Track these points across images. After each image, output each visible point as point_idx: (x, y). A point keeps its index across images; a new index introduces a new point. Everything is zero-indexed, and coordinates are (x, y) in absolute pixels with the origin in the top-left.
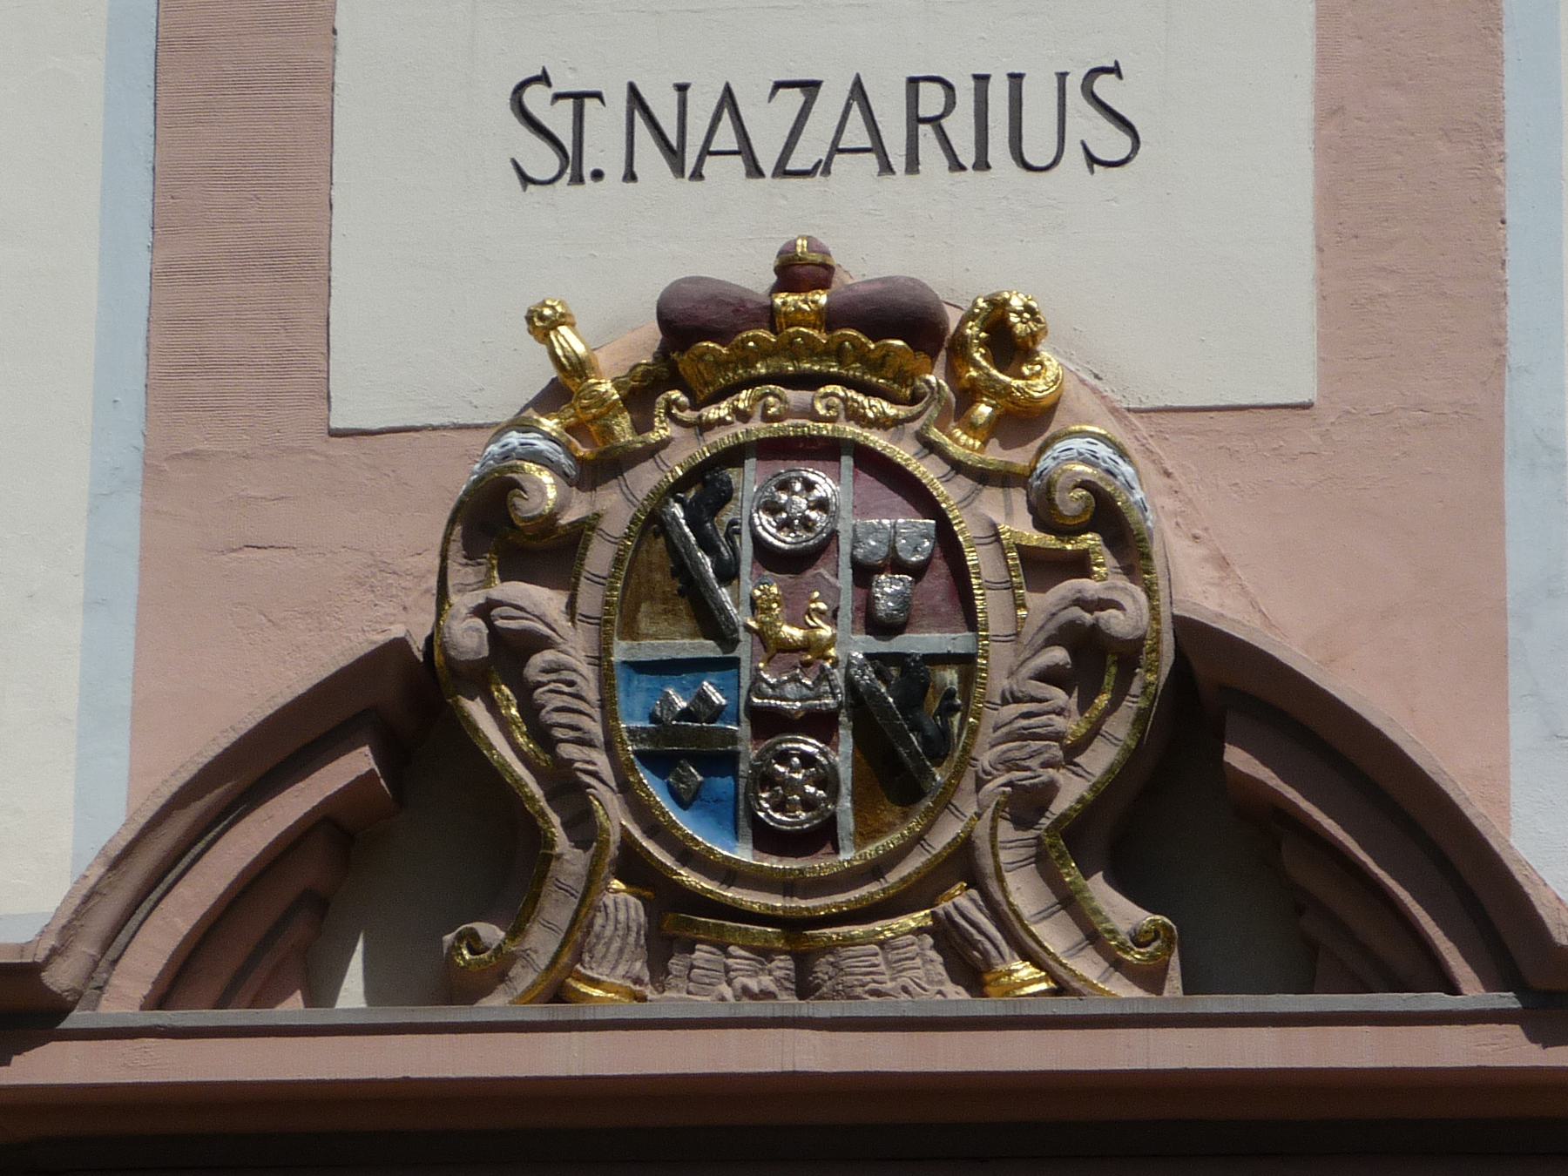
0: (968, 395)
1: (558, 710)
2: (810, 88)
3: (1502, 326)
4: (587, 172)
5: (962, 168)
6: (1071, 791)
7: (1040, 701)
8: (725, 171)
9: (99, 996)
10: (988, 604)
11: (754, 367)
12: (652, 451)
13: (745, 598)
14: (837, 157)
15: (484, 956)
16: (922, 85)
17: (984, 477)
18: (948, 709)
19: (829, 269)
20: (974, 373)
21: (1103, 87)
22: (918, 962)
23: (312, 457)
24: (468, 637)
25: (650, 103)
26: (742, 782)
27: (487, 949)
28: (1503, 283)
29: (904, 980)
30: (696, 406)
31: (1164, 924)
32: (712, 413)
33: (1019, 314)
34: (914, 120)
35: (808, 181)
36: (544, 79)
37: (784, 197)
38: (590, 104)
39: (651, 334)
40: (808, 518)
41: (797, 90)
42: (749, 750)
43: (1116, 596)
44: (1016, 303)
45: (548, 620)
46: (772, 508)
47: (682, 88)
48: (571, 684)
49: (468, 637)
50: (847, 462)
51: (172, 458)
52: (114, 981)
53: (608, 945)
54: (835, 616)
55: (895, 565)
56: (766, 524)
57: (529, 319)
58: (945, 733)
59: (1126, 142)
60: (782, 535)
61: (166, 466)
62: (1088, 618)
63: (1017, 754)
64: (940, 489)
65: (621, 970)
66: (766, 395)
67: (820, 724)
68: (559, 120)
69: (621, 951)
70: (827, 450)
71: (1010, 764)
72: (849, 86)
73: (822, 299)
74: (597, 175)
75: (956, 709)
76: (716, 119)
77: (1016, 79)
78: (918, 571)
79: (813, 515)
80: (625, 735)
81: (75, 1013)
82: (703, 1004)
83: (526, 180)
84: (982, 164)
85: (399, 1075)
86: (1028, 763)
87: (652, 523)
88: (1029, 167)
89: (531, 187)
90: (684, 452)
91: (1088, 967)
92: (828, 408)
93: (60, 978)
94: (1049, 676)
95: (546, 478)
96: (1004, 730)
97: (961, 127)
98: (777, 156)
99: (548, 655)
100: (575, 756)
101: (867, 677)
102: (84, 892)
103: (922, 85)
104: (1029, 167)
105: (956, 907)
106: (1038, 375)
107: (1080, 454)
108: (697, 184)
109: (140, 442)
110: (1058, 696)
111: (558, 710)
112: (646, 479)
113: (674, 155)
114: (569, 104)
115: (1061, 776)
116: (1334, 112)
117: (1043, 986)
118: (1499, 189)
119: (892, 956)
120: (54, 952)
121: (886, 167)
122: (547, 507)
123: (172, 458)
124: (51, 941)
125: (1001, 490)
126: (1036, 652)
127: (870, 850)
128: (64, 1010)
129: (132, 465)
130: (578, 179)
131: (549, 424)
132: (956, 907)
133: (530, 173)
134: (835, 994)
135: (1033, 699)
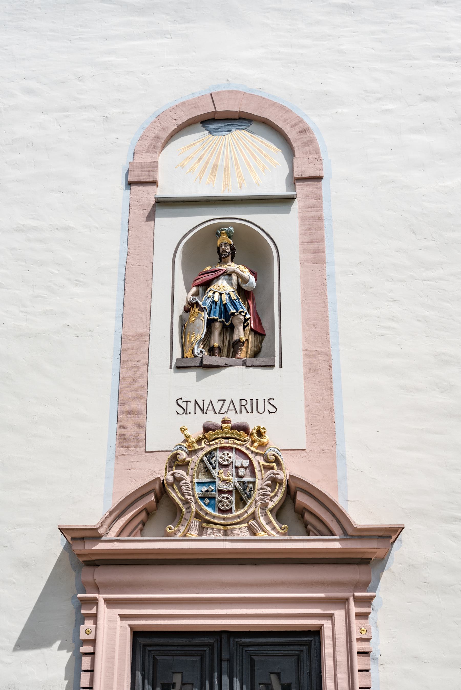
0: (253, 442)
1: (185, 490)
4: (188, 413)
5: (249, 413)
6: (271, 505)
8: (211, 413)
9: (107, 535)
10: (258, 474)
11: (219, 435)
12: (202, 449)
13: (217, 472)
14: (228, 411)
15: (172, 530)
16: (242, 400)
17: (257, 454)
18: (251, 490)
19: (231, 421)
20: (255, 438)
21: (271, 401)
22: (245, 532)
23: (143, 455)
24: (170, 479)
25: (198, 402)
26: (216, 502)
27: (172, 529)
30: (209, 442)
31: (286, 526)
32: (211, 443)
33: (262, 429)
35: (224, 414)
36: (181, 399)
37: (220, 417)
39: (202, 431)
40: (228, 459)
41: (222, 401)
42: (218, 498)
43: (279, 473)
44: (262, 427)
45: (184, 475)
46: (222, 458)
47: (203, 400)
48: (188, 486)
49: (170, 479)
50: (234, 450)
52: (110, 532)
53: (193, 528)
54: (232, 475)
55: (242, 467)
56: (221, 460)
57: (181, 429)
58: (250, 495)
59: (275, 410)
60: (223, 462)
61: (119, 456)
62: (274, 476)
63: (262, 498)
66: (220, 440)
67: (229, 492)
68: (184, 405)
69: (195, 529)
70: (231, 449)
71: (261, 499)
73: (230, 425)
74: (190, 413)
75: (252, 490)
76: (209, 405)
78: (246, 468)
79: (229, 459)
80: (197, 494)
81: (103, 537)
83: (178, 414)
85: (158, 548)
86: (264, 499)
87: (202, 461)
89: (179, 415)
90: (207, 449)
91: (273, 533)
92: (231, 442)
93: (101, 531)
94: (267, 485)
95: (184, 453)
96: (261, 494)
97: (248, 407)
98: (219, 410)
99: (184, 481)
100: (188, 497)
102: (105, 517)
103: (242, 400)
105: (252, 523)
106: (265, 439)
107: (273, 450)
108: (206, 415)
110: (269, 489)
111: (185, 490)
112: (201, 454)
113: (202, 410)
115: (270, 502)
116: (307, 406)
118: (334, 418)
119: (241, 530)
120: (100, 527)
122: (184, 458)
124: (100, 525)
125: (259, 457)
128: (101, 537)
129: (113, 456)
131: (185, 445)
132: (252, 523)
133: (179, 413)
135: (265, 489)
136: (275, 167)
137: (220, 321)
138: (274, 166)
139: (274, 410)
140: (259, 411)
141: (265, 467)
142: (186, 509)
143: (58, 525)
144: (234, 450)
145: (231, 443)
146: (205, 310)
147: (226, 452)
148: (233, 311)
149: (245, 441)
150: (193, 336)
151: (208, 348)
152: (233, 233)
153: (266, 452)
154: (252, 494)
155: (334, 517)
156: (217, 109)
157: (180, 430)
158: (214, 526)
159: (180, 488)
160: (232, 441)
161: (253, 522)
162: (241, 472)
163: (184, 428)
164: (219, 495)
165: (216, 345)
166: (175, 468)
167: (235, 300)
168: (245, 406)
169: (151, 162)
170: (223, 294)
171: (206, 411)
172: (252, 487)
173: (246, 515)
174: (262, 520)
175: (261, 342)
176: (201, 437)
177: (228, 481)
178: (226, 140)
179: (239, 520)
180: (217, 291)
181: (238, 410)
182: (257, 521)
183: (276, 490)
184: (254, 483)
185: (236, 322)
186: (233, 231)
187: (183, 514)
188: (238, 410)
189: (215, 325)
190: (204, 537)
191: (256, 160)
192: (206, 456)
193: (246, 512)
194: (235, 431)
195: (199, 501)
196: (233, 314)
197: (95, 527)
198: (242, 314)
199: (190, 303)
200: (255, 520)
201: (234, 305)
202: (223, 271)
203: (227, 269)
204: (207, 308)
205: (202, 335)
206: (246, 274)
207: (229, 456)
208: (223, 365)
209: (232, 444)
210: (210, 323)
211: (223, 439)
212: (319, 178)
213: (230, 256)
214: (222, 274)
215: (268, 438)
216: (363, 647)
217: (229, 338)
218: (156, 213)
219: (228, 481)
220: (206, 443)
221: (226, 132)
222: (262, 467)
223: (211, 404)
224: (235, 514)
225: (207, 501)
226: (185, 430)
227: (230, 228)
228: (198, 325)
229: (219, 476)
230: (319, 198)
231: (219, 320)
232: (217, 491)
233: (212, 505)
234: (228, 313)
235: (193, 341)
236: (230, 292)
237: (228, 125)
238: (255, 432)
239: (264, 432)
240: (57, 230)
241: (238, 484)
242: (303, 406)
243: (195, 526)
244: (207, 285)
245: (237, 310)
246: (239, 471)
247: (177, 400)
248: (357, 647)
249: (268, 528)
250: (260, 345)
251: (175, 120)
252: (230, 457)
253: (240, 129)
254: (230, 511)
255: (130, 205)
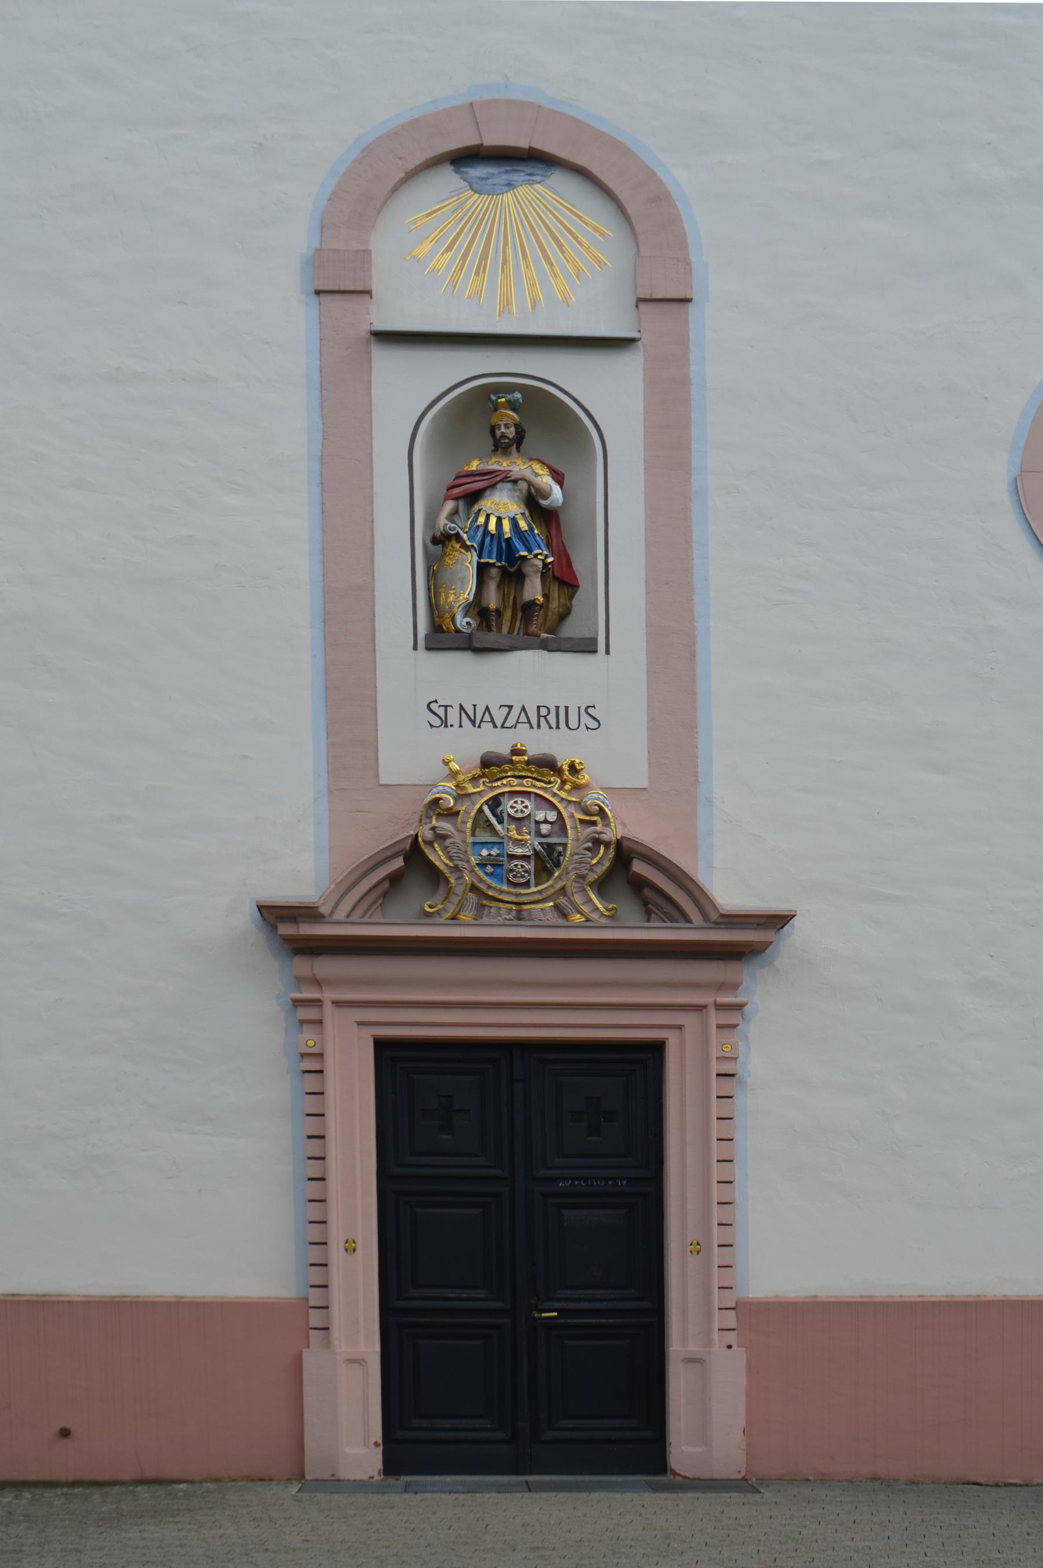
0: (564, 782)
2: (510, 707)
3: (697, 772)
4: (449, 725)
5: (552, 728)
6: (593, 877)
7: (585, 855)
8: (487, 726)
14: (518, 724)
16: (541, 708)
21: (590, 710)
25: (466, 710)
28: (697, 762)
29: (547, 917)
30: (490, 782)
34: (539, 716)
36: (436, 701)
38: (448, 708)
41: (506, 708)
43: (605, 831)
46: (512, 807)
47: (475, 706)
48: (458, 847)
50: (533, 796)
51: (336, 790)
54: (530, 833)
55: (546, 822)
56: (511, 812)
57: (443, 760)
62: (597, 836)
63: (578, 867)
64: (558, 805)
65: (471, 913)
68: (441, 712)
70: (526, 794)
71: (578, 869)
72: (521, 707)
74: (452, 726)
75: (562, 856)
76: (521, 713)
77: (567, 708)
79: (524, 809)
82: (494, 921)
83: (432, 726)
84: (558, 727)
88: (571, 729)
89: (433, 728)
93: (325, 910)
99: (451, 840)
101: (539, 848)
103: (541, 708)
104: (571, 729)
106: (582, 779)
109: (327, 785)
110: (589, 854)
111: (455, 853)
113: (473, 722)
114: (443, 708)
117: (583, 919)
118: (696, 740)
119: (544, 912)
121: (531, 727)
123: (336, 790)
126: (584, 844)
127: (540, 888)
130: (446, 726)
133: (433, 724)
134: (529, 920)
135: (583, 854)
136: (600, 267)
137: (498, 567)
138: (597, 264)
139: (596, 725)
140: (570, 726)
141: (582, 821)
142: (457, 879)
143: (257, 902)
144: (533, 796)
145: (527, 786)
146: (473, 550)
147: (519, 800)
148: (524, 553)
149: (550, 782)
150: (452, 592)
151: (476, 610)
152: (520, 404)
153: (584, 800)
154: (562, 861)
155: (690, 897)
156: (484, 140)
157: (441, 761)
158: (501, 905)
159: (445, 849)
160: (529, 783)
161: (563, 900)
162: (545, 828)
163: (448, 758)
164: (509, 861)
165: (493, 606)
166: (436, 819)
167: (526, 531)
168: (547, 717)
169: (357, 251)
170: (504, 518)
171: (480, 723)
172: (562, 850)
173: (552, 891)
174: (578, 899)
175: (571, 597)
176: (476, 774)
177: (523, 843)
178: (504, 204)
179: (540, 897)
180: (493, 512)
181: (534, 723)
182: (569, 898)
183: (600, 855)
184: (565, 845)
185: (527, 569)
186: (521, 401)
187: (451, 887)
188: (534, 723)
189: (489, 572)
190: (485, 920)
191: (563, 252)
192: (487, 804)
193: (552, 886)
194: (533, 768)
195: (477, 869)
196: (524, 558)
197: (315, 906)
198: (540, 557)
199: (445, 535)
200: (566, 898)
201: (525, 540)
202: (503, 475)
203: (510, 471)
204: (475, 545)
205: (468, 594)
206: (546, 480)
207: (524, 805)
208: (507, 648)
209: (528, 787)
210: (482, 569)
211: (514, 779)
212: (687, 301)
213: (515, 445)
214: (502, 481)
215: (587, 777)
216: (726, 1068)
217: (515, 593)
218: (373, 357)
219: (523, 843)
220: (488, 785)
221: (503, 188)
222: (578, 822)
223: (487, 713)
224: (533, 889)
225: (489, 869)
226: (450, 761)
227: (516, 396)
228: (460, 575)
229: (509, 835)
230: (683, 342)
231: (499, 564)
232: (505, 855)
233: (497, 875)
234: (514, 555)
235: (453, 603)
236: (516, 515)
237: (507, 172)
238: (566, 768)
239: (582, 769)
240: (183, 382)
241: (540, 847)
242: (645, 719)
243: (471, 904)
244: (474, 497)
245: (530, 551)
246: (541, 828)
247: (429, 704)
248: (715, 1068)
249: (585, 909)
250: (568, 604)
251: (400, 158)
252: (526, 807)
253: (531, 182)
254: (527, 884)
255: (322, 338)
